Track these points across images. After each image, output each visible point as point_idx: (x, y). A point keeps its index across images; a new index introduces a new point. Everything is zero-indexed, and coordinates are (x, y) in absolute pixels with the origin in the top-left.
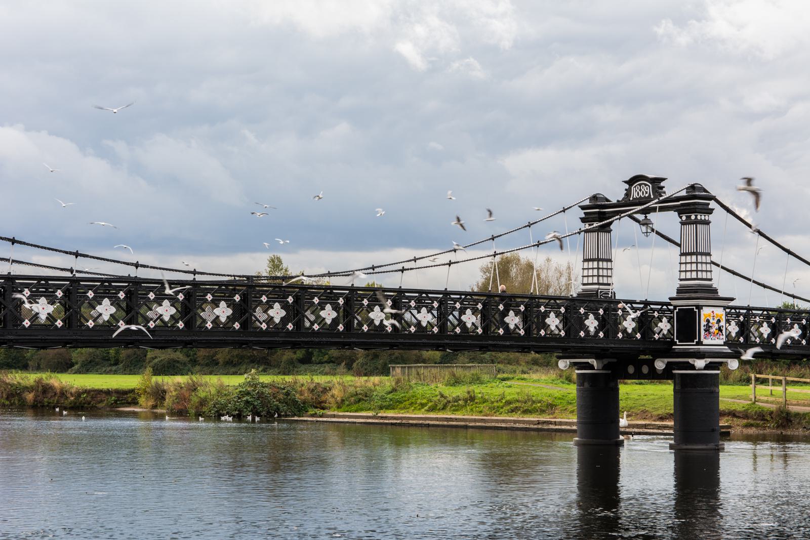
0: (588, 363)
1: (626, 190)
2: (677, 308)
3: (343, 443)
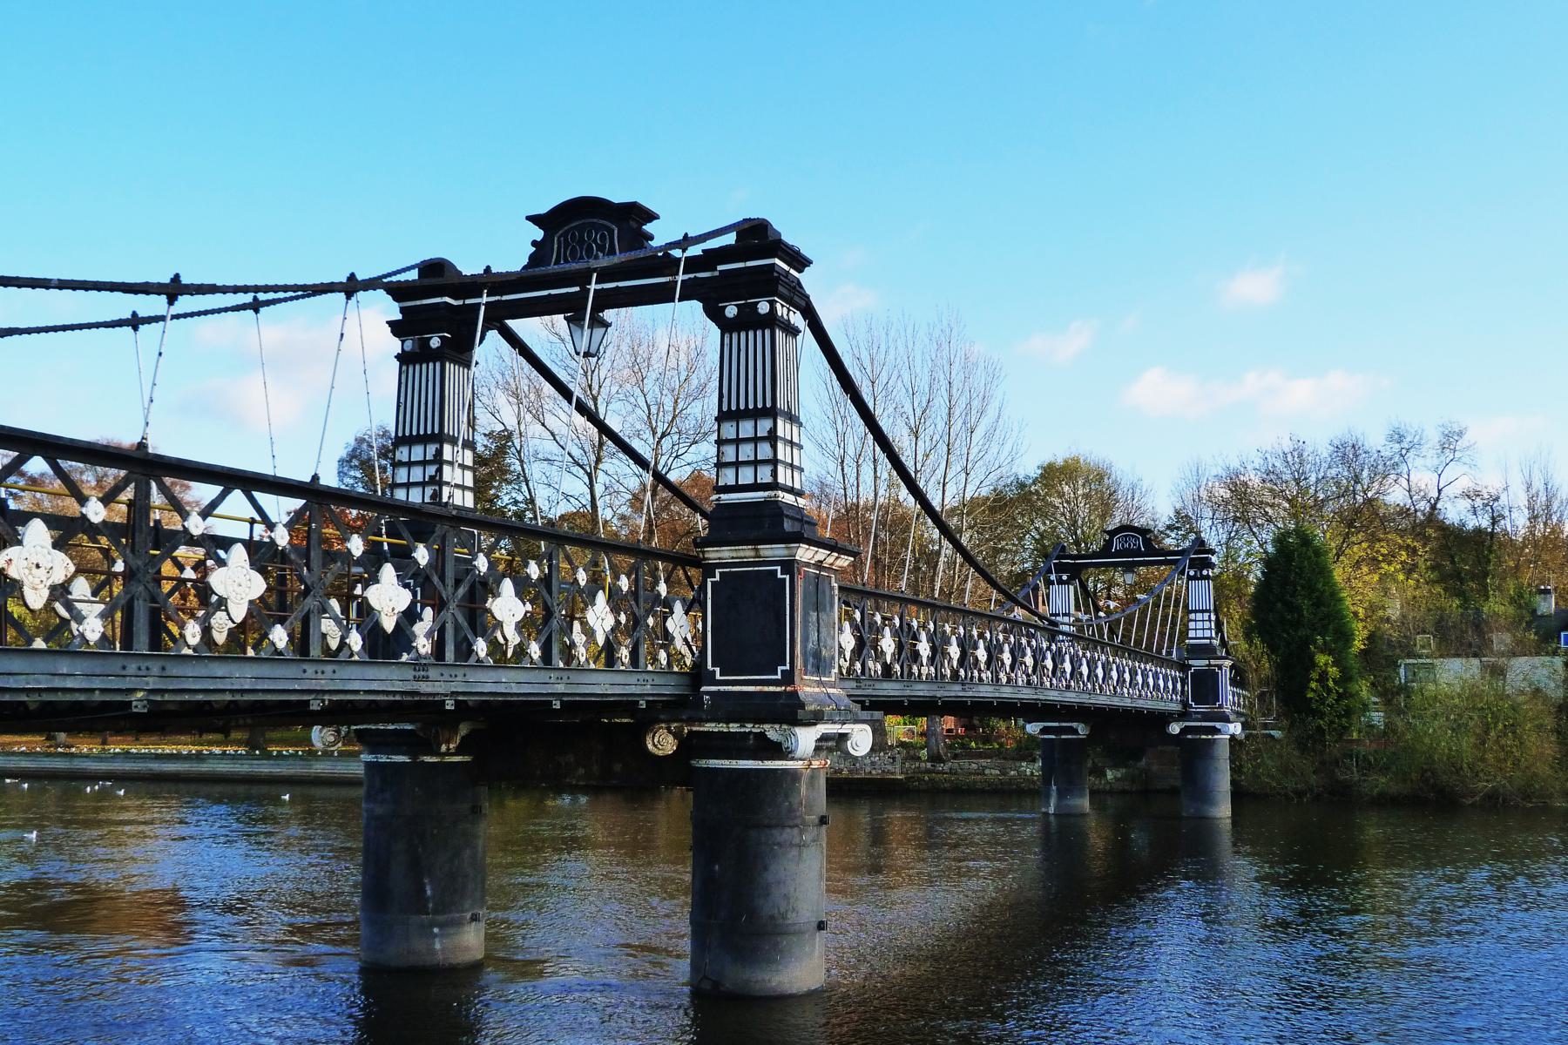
0: (1071, 727)
1: (534, 243)
2: (788, 577)
3: (779, 883)
